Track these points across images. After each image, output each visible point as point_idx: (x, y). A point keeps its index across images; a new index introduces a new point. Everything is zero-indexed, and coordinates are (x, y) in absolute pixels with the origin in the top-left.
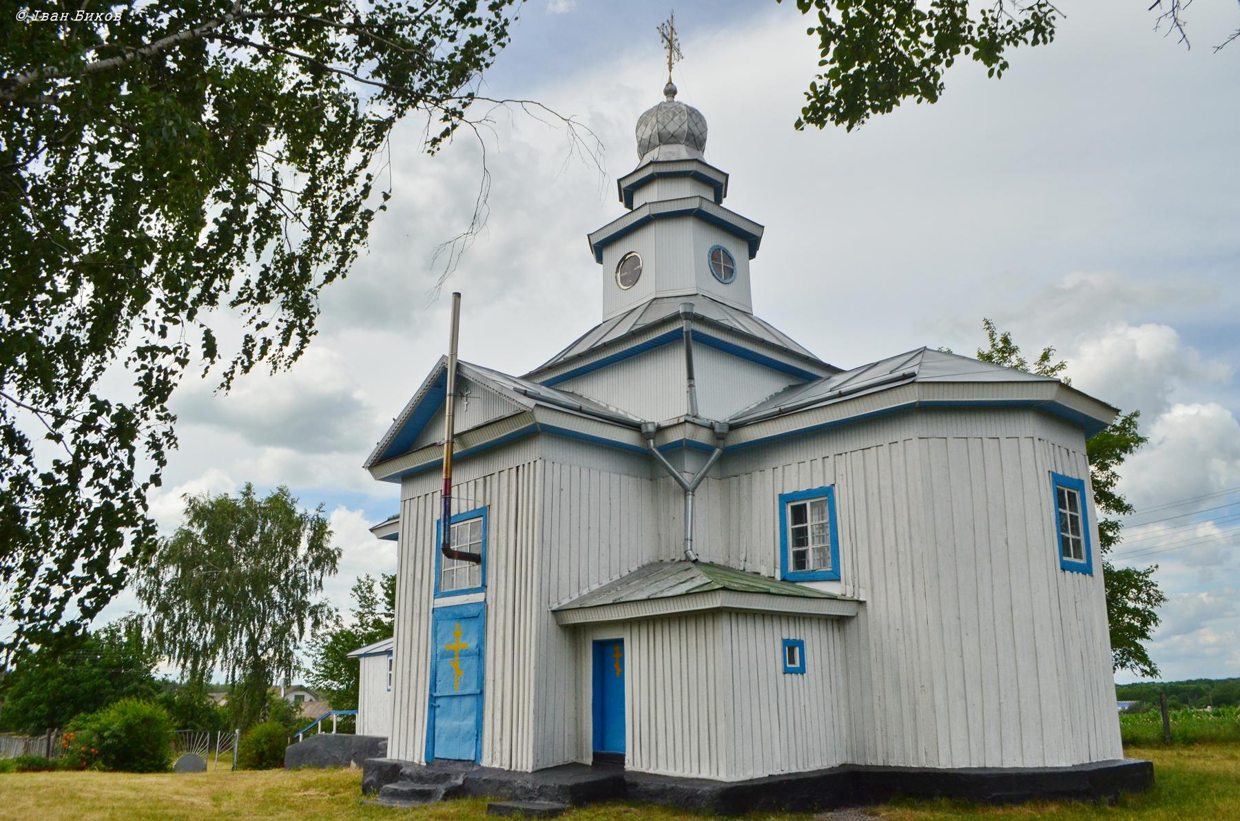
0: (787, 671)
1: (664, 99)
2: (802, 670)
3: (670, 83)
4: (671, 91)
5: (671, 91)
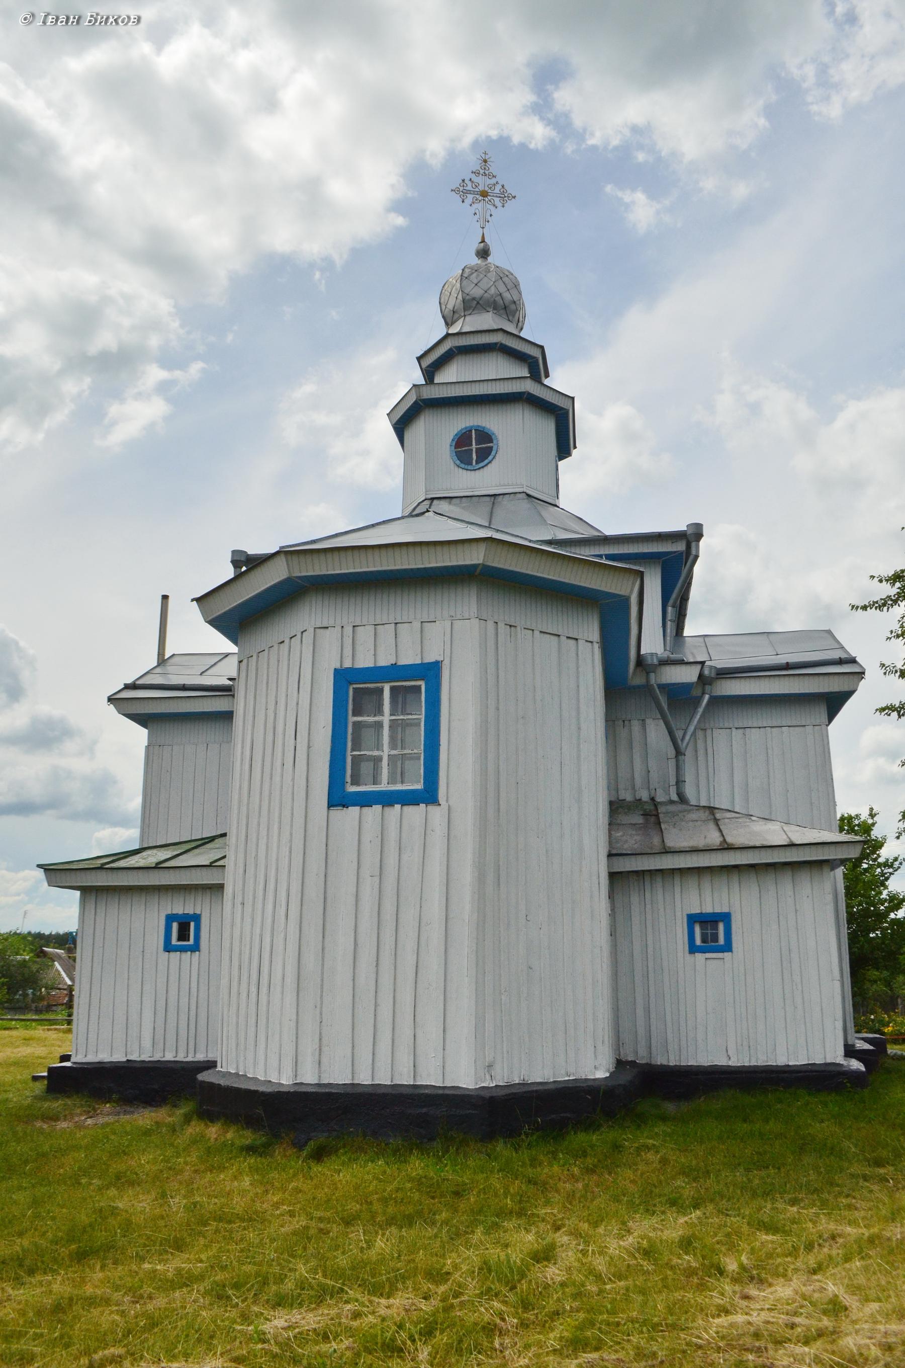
0: (168, 948)
1: (475, 261)
2: (196, 948)
3: (483, 241)
4: (484, 253)
5: (484, 253)
